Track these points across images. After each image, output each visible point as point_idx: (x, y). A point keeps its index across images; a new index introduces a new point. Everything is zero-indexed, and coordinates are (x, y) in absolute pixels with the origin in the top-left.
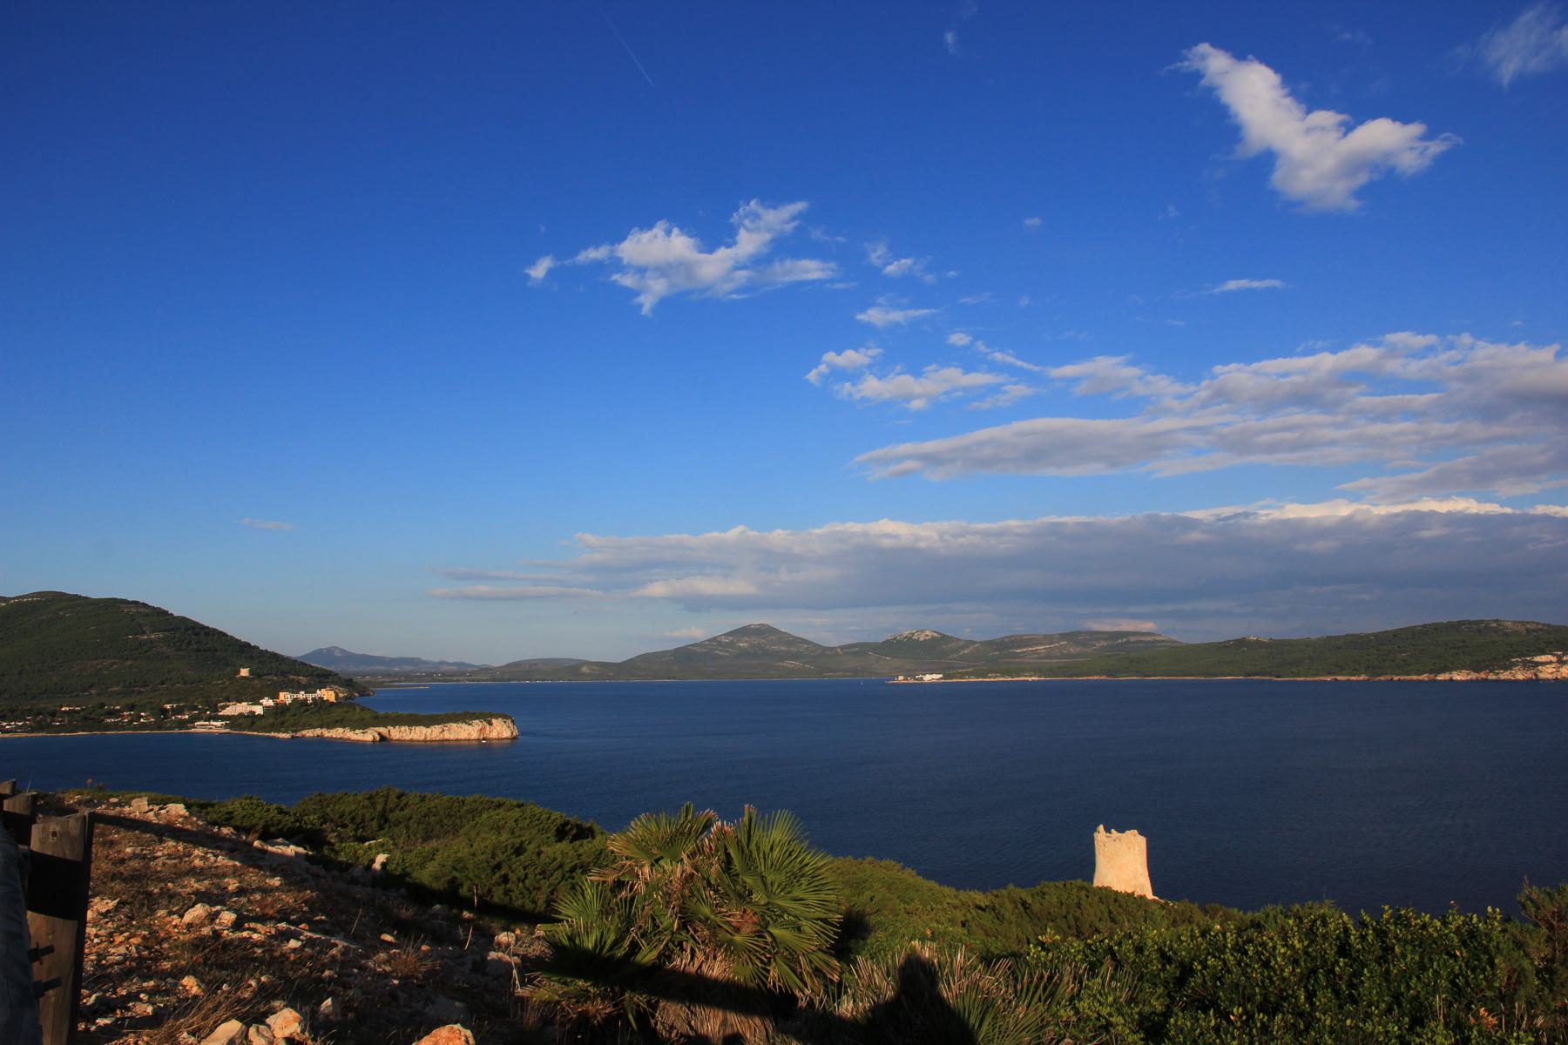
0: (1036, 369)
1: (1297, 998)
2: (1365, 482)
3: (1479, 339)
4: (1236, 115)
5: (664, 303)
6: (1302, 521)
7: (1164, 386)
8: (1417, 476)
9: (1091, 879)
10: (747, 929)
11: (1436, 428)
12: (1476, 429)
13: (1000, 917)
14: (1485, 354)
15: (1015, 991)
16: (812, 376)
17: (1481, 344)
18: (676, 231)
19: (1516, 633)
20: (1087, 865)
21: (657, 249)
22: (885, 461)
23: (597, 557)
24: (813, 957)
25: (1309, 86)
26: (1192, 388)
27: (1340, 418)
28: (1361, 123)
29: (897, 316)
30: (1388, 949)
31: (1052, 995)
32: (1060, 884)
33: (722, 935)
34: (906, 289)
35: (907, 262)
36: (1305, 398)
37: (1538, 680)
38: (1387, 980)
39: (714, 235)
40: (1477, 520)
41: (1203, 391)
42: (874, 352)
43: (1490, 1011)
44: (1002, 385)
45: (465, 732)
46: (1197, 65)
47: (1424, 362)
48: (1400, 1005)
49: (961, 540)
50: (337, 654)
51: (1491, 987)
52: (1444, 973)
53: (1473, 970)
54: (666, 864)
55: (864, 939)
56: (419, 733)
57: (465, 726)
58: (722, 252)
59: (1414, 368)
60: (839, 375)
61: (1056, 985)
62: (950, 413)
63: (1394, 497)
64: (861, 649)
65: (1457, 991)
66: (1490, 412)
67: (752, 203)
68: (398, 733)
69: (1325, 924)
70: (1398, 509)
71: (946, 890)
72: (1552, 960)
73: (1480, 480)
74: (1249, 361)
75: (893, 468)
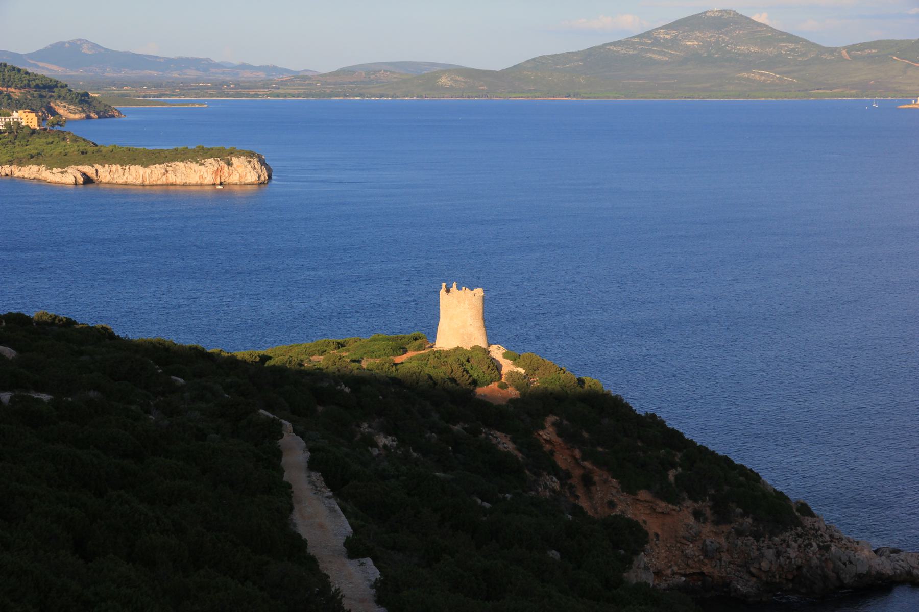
9: (485, 300)
45: (195, 174)
50: (85, 50)
56: (135, 175)
57: (195, 166)
68: (110, 174)
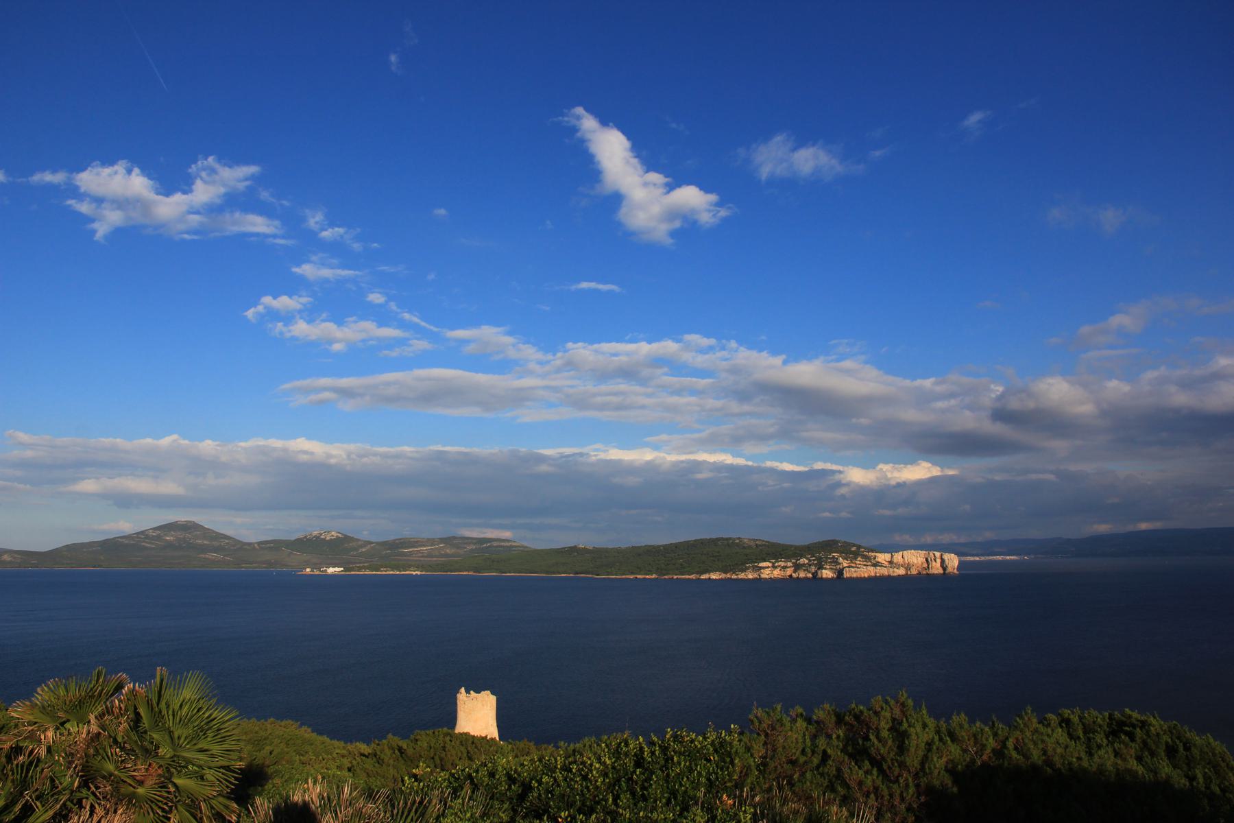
0: (435, 329)
1: (607, 801)
2: (664, 437)
3: (741, 345)
4: (599, 162)
5: (119, 233)
6: (620, 461)
7: (530, 352)
8: (696, 435)
10: (150, 782)
11: (711, 403)
12: (735, 407)
13: (380, 762)
14: (744, 356)
15: (392, 815)
16: (250, 313)
17: (742, 348)
18: (136, 171)
19: (750, 547)
20: (452, 719)
21: (116, 186)
22: (307, 391)
23: (29, 453)
24: (214, 802)
25: (649, 153)
26: (550, 357)
27: (650, 390)
28: (680, 186)
29: (326, 273)
30: (668, 759)
31: (423, 815)
32: (430, 732)
33: (125, 789)
34: (336, 250)
35: (341, 230)
36: (628, 373)
38: (667, 782)
39: (172, 180)
40: (731, 468)
41: (558, 360)
42: (304, 300)
43: (729, 796)
44: (408, 339)
46: (573, 122)
47: (707, 356)
48: (675, 799)
49: (365, 460)
51: (730, 781)
52: (704, 773)
53: (722, 769)
54: (72, 727)
55: (262, 786)
58: (178, 197)
59: (701, 360)
60: (273, 315)
61: (426, 808)
62: (362, 358)
63: (680, 449)
64: (275, 545)
65: (710, 784)
66: (743, 396)
67: (211, 159)
69: (627, 745)
70: (683, 457)
71: (336, 743)
72: (765, 757)
73: (735, 441)
74: (592, 343)
75: (313, 397)
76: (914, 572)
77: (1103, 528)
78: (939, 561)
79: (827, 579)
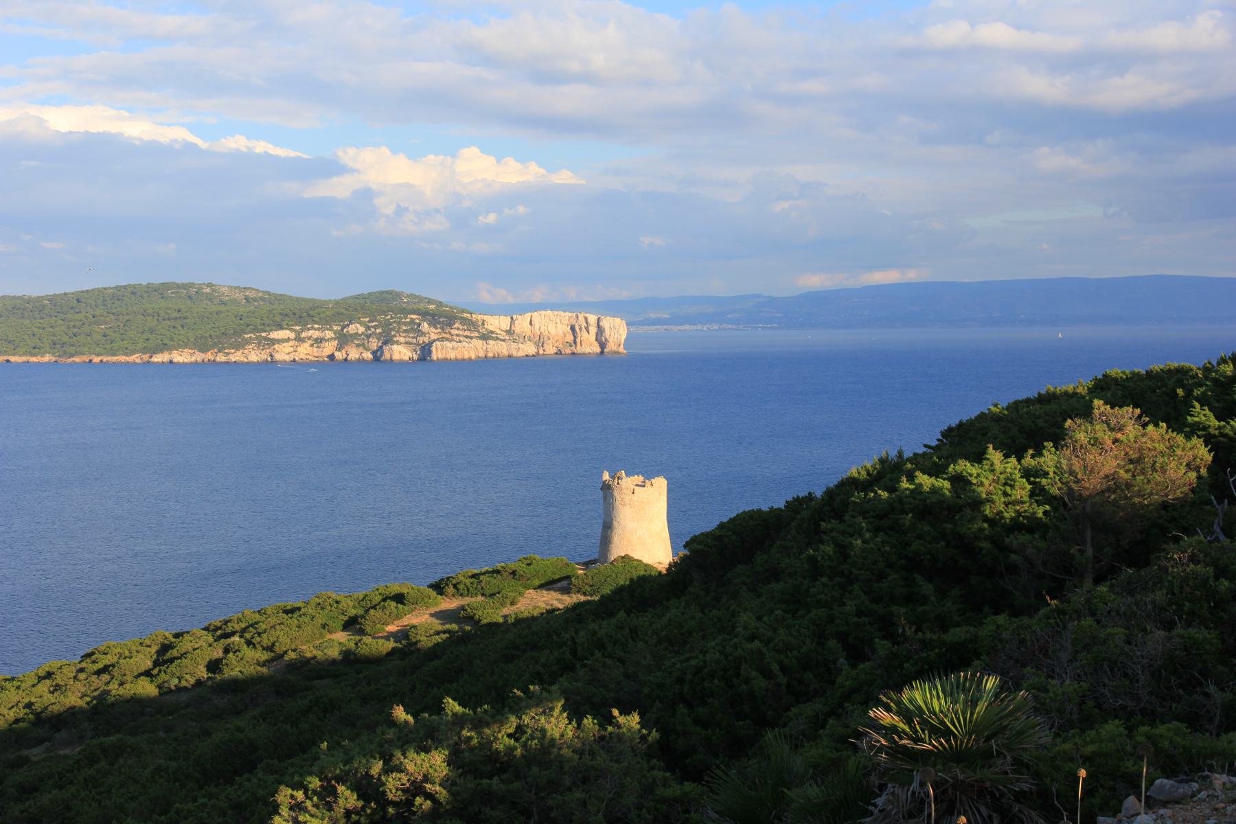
37: (273, 362)
76: (550, 350)
77: (814, 281)
78: (593, 330)
79: (402, 363)
